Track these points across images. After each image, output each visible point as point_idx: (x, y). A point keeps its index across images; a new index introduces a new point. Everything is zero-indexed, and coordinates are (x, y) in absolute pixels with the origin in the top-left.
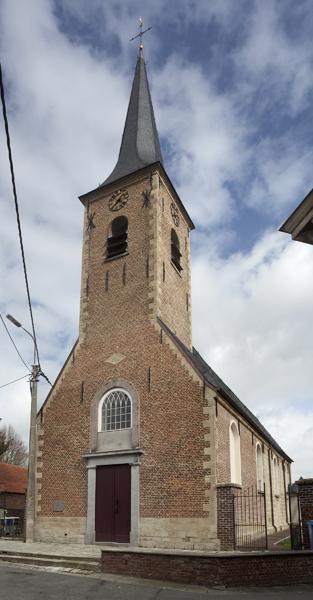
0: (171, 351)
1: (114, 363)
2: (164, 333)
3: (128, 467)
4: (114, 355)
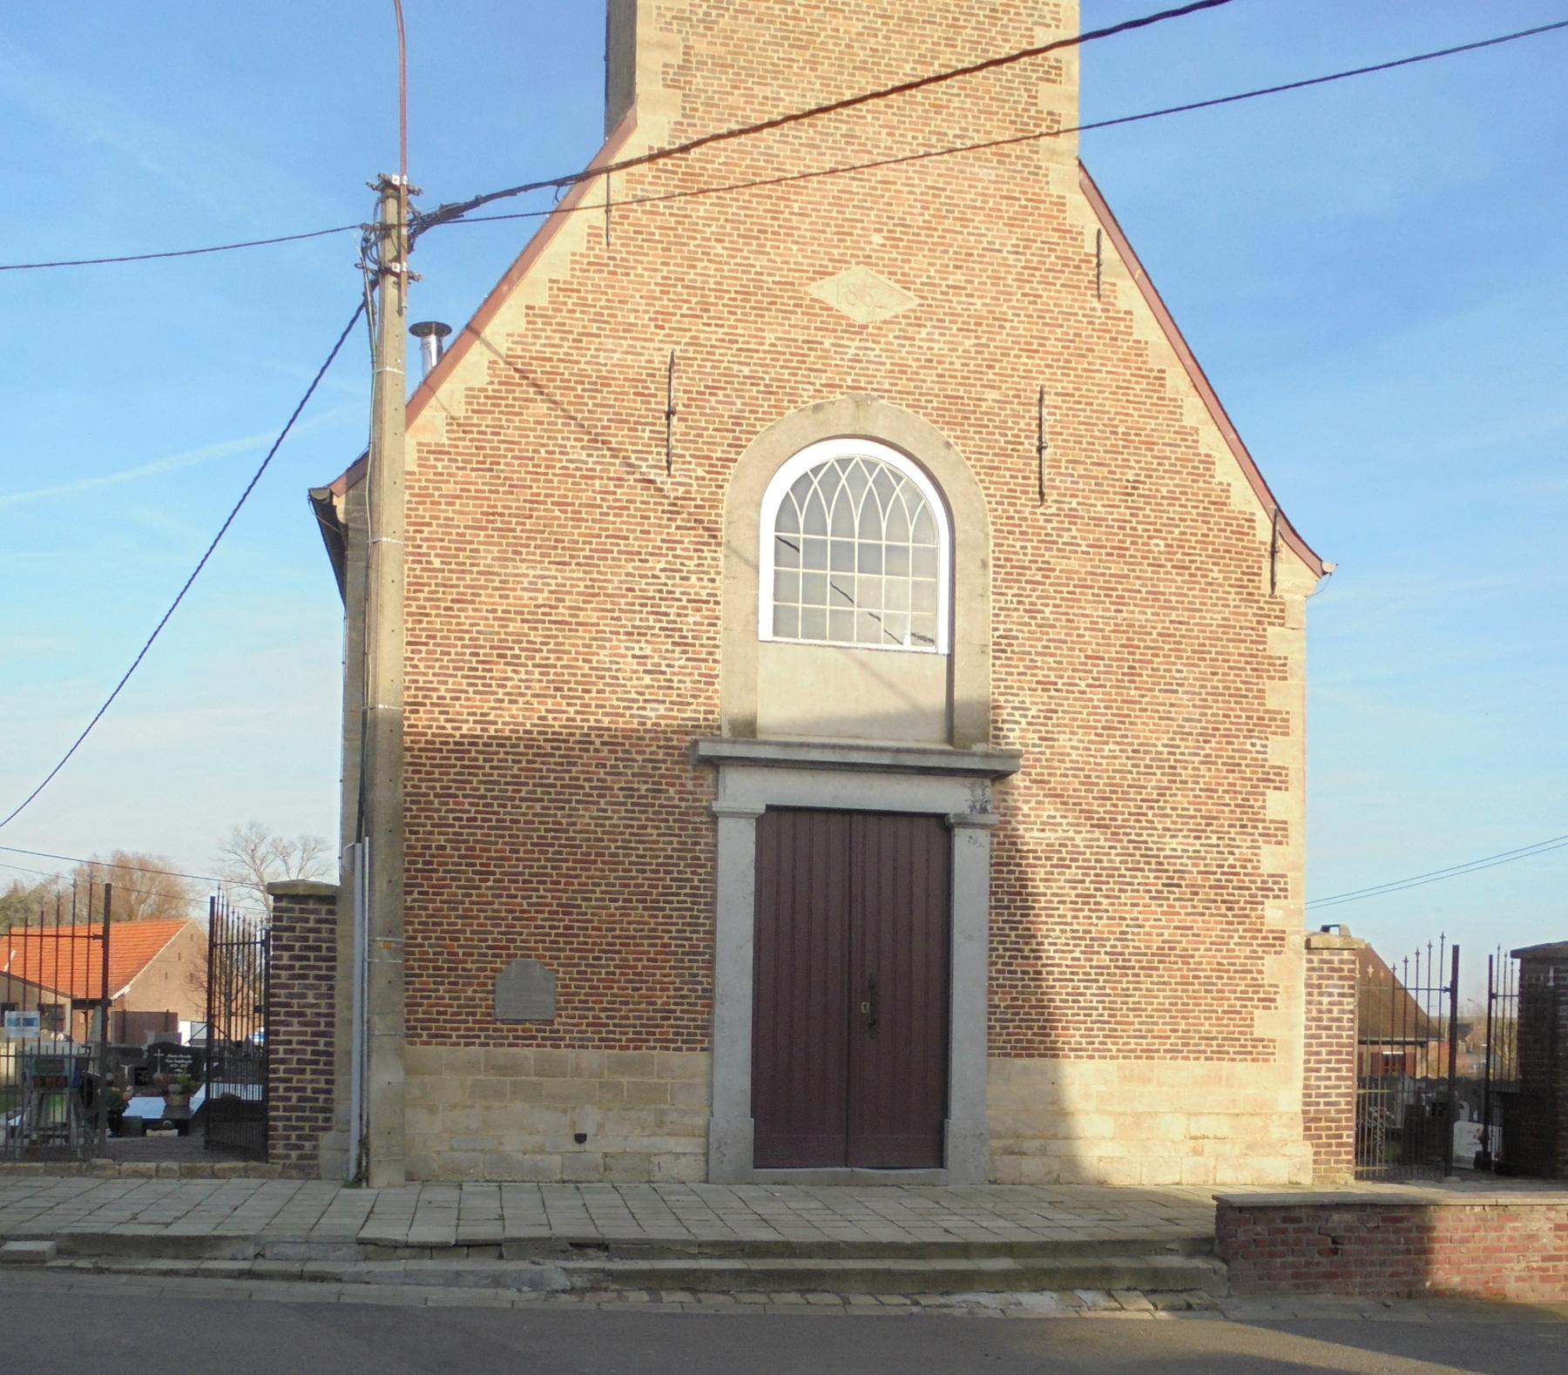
0: (1140, 348)
1: (859, 315)
3: (943, 825)
4: (855, 275)
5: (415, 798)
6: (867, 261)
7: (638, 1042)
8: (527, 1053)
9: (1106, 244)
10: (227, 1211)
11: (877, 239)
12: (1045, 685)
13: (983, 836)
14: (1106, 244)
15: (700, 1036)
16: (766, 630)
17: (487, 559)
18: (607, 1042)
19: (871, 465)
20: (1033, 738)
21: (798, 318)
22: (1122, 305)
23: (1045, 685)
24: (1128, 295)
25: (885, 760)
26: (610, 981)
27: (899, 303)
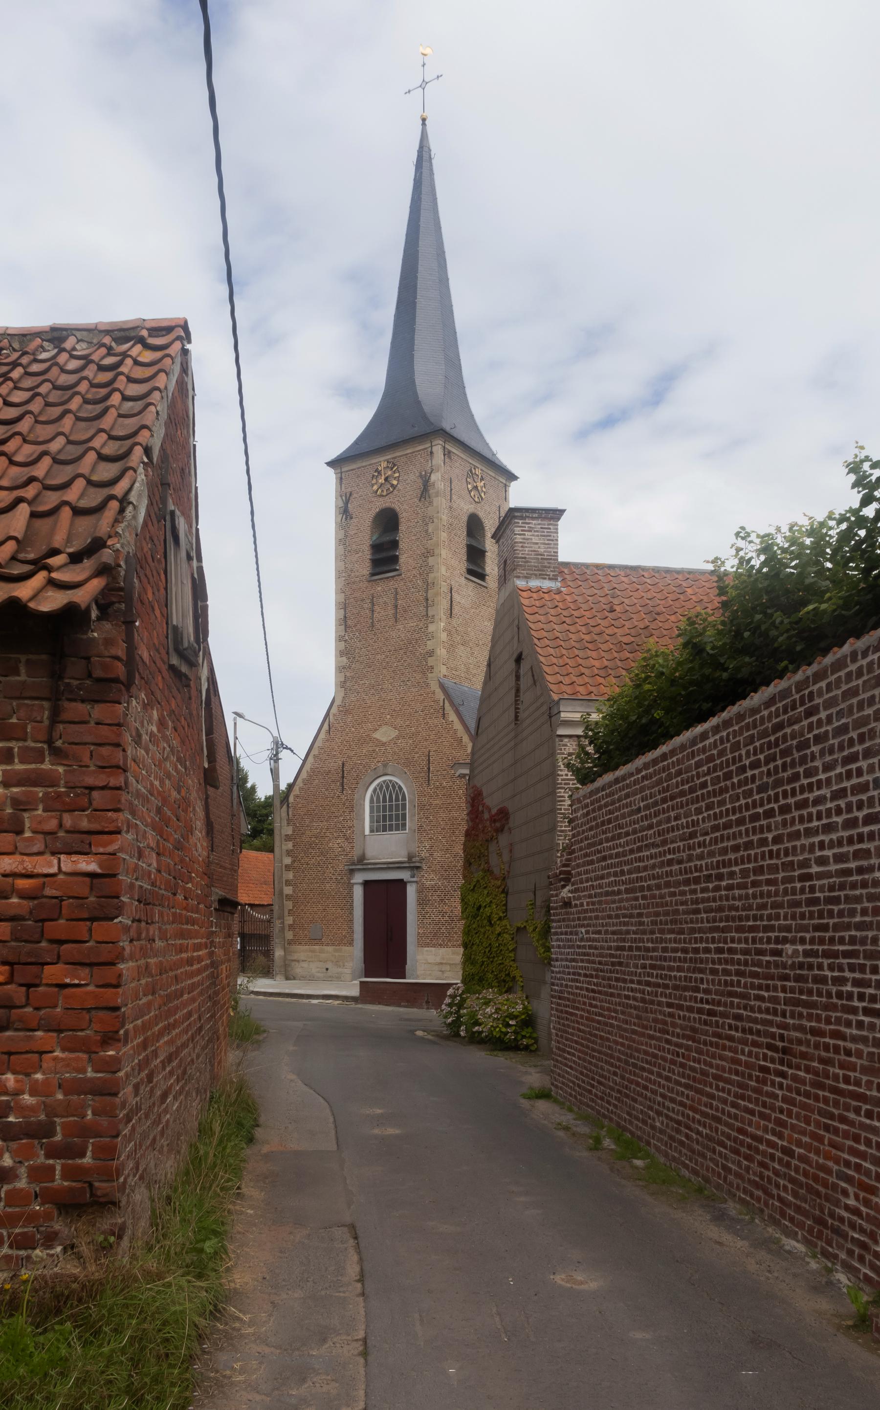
0: (456, 731)
1: (384, 740)
2: (447, 704)
3: (401, 885)
4: (384, 729)
5: (571, 821)
6: (386, 724)
7: (339, 945)
8: (317, 947)
9: (446, 701)
10: (143, 681)
11: (388, 717)
12: (431, 839)
13: (414, 885)
14: (446, 701)
15: (351, 943)
16: (367, 832)
17: (307, 822)
18: (333, 945)
19: (391, 781)
20: (427, 855)
21: (371, 744)
22: (450, 719)
23: (431, 839)
24: (452, 717)
25: (397, 865)
26: (333, 928)
27: (394, 733)
